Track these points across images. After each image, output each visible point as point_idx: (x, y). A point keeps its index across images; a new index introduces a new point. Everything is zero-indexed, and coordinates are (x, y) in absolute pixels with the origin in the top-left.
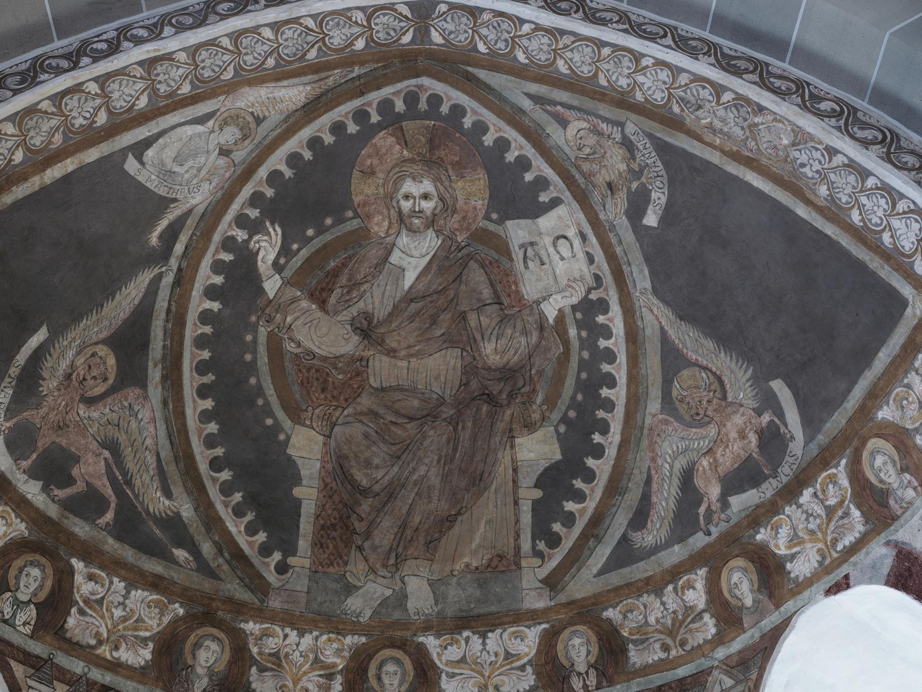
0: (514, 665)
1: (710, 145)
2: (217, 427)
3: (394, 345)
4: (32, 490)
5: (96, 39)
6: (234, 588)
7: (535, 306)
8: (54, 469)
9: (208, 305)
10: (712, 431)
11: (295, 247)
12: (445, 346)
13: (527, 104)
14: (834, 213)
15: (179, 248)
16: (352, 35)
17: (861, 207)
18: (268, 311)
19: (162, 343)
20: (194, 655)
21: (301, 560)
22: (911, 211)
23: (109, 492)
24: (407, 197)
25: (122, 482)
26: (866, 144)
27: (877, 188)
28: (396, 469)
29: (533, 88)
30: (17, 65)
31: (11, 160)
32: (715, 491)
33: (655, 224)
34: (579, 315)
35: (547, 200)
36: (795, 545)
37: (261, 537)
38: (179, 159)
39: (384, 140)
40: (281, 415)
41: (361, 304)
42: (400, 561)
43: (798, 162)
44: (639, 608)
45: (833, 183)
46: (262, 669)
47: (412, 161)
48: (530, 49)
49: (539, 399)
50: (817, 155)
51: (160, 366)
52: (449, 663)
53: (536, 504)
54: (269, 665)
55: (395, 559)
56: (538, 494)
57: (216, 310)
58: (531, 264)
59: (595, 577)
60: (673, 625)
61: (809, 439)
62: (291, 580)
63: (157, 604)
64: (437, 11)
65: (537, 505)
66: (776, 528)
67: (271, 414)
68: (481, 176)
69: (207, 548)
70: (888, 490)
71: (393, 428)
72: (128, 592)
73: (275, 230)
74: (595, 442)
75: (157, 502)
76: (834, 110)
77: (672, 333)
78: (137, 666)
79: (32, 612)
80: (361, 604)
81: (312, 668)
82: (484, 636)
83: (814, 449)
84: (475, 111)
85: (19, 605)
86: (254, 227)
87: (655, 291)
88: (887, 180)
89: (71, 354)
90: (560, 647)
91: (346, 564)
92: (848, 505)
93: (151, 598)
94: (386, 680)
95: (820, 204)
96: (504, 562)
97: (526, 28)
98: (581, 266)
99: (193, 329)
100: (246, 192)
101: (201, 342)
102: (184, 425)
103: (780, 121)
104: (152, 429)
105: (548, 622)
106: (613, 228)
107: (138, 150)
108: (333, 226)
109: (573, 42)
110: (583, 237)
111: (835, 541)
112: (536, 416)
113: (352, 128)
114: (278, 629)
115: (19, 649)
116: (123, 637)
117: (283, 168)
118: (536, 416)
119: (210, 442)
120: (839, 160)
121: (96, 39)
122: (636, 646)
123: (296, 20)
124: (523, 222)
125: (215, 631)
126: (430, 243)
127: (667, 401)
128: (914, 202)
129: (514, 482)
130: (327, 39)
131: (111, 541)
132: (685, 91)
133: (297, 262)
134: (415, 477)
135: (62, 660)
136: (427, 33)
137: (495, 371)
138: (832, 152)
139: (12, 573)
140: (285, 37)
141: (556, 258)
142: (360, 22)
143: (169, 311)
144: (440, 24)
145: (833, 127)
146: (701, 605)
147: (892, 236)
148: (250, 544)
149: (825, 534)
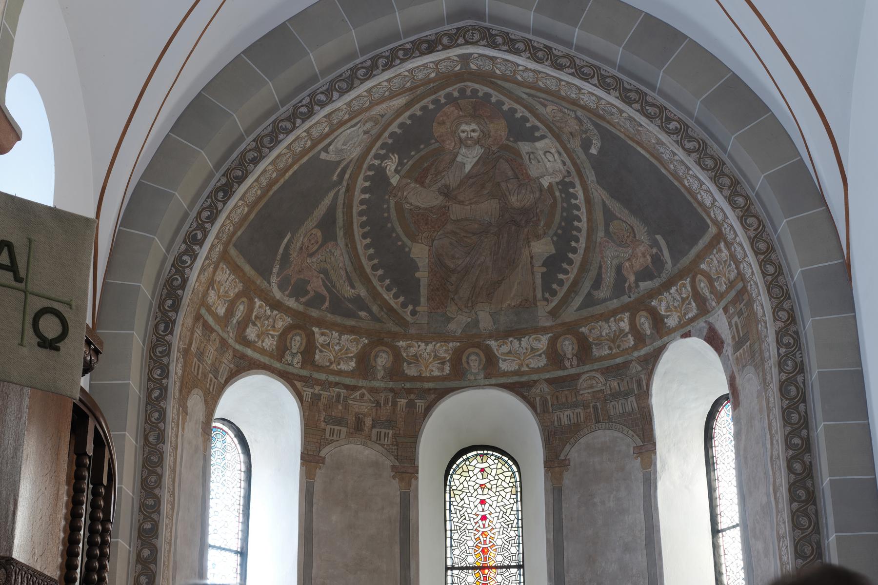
3: (462, 199)
4: (291, 303)
8: (299, 290)
9: (363, 196)
13: (525, 96)
15: (347, 176)
21: (423, 308)
23: (325, 293)
24: (463, 132)
28: (468, 259)
29: (527, 91)
32: (632, 278)
34: (560, 187)
37: (402, 299)
38: (344, 144)
39: (449, 109)
40: (405, 239)
41: (443, 181)
47: (465, 116)
49: (542, 223)
52: (503, 354)
53: (543, 274)
56: (544, 270)
61: (674, 265)
63: (355, 340)
66: (660, 301)
67: (401, 240)
69: (375, 309)
76: (676, 128)
79: (299, 356)
80: (455, 327)
81: (434, 360)
82: (520, 340)
85: (293, 355)
86: (383, 158)
87: (598, 182)
90: (558, 345)
94: (472, 364)
97: (520, 68)
99: (356, 208)
101: (361, 214)
102: (357, 253)
104: (342, 259)
106: (574, 151)
107: (326, 149)
110: (560, 154)
111: (685, 314)
112: (541, 232)
113: (431, 107)
115: (297, 375)
116: (341, 358)
118: (541, 232)
119: (370, 258)
120: (676, 158)
124: (527, 143)
125: (384, 348)
131: (329, 315)
133: (407, 167)
134: (479, 262)
135: (316, 375)
136: (468, 64)
138: (675, 154)
139: (288, 341)
143: (344, 203)
146: (627, 330)
148: (396, 303)
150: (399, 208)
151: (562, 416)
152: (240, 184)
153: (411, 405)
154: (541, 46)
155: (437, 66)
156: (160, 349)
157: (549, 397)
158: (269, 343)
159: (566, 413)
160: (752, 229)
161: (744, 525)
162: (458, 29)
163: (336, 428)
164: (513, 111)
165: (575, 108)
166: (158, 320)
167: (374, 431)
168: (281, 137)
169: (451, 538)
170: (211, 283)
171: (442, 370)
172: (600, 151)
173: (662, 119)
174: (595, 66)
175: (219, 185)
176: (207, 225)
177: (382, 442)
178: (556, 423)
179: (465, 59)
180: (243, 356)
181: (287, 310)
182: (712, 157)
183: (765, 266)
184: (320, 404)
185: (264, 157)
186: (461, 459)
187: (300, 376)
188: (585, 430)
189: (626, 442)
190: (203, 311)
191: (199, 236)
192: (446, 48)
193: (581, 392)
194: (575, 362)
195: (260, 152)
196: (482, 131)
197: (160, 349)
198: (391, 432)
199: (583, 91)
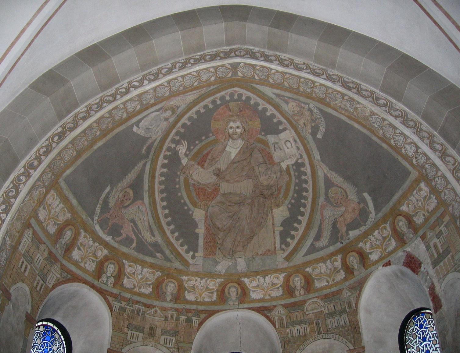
0: (275, 287)
1: (341, 113)
2: (168, 211)
4: (109, 239)
5: (121, 87)
6: (177, 265)
7: (278, 164)
10: (343, 209)
11: (192, 147)
12: (247, 178)
14: (384, 139)
16: (210, 76)
17: (394, 139)
18: (183, 170)
19: (148, 185)
20: (166, 289)
21: (200, 254)
22: (412, 143)
23: (133, 237)
24: (231, 128)
25: (137, 231)
26: (396, 117)
27: (400, 134)
30: (95, 100)
31: (96, 135)
32: (344, 229)
33: (321, 138)
34: (294, 168)
35: (282, 128)
36: (372, 249)
41: (216, 165)
42: (234, 253)
43: (372, 121)
44: (318, 268)
45: (384, 130)
46: (189, 292)
48: (274, 78)
50: (378, 120)
51: (147, 193)
52: (252, 287)
54: (191, 290)
55: (232, 253)
56: (281, 228)
57: (166, 172)
58: (277, 150)
59: (302, 257)
60: (330, 273)
62: (197, 261)
64: (240, 66)
65: (281, 233)
66: (365, 243)
67: (187, 205)
68: (258, 120)
69: (167, 252)
70: (404, 233)
71: (229, 207)
72: (143, 269)
73: (185, 143)
74: (301, 210)
75: (148, 237)
76: (384, 103)
77: (328, 175)
78: (147, 293)
79: (112, 279)
82: (264, 277)
83: (380, 215)
84: (254, 99)
85: (108, 278)
86: (178, 143)
87: (322, 161)
88: (403, 131)
89: (118, 193)
91: (215, 254)
92: (390, 238)
93: (150, 270)
94: (231, 294)
95: (380, 136)
96: (271, 252)
98: (294, 151)
100: (174, 131)
101: (160, 183)
103: (365, 108)
105: (287, 272)
107: (137, 123)
108: (205, 139)
109: (290, 77)
110: (295, 141)
113: (211, 106)
114: (193, 278)
116: (142, 285)
117: (187, 122)
120: (386, 122)
121: (121, 87)
122: (317, 280)
123: (190, 74)
126: (240, 143)
127: (327, 198)
128: (413, 140)
129: (273, 224)
130: (201, 78)
131: (136, 253)
132: (331, 95)
137: (265, 186)
138: (384, 120)
140: (186, 79)
141: (285, 148)
142: (212, 71)
143: (149, 173)
144: (241, 70)
145: (384, 111)
146: (340, 267)
147: (405, 150)
149: (382, 246)
150: (186, 180)
152: (70, 132)
153: (189, 321)
154: (287, 59)
157: (284, 318)
158: (91, 266)
159: (296, 328)
160: (451, 164)
162: (231, 49)
163: (136, 333)
164: (265, 110)
165: (309, 101)
167: (163, 338)
168: (105, 105)
170: (41, 202)
171: (211, 297)
172: (324, 136)
173: (373, 98)
174: (324, 69)
175: (56, 132)
176: (42, 157)
177: (168, 345)
178: (290, 336)
179: (235, 66)
180: (69, 272)
182: (412, 120)
184: (125, 314)
185: (91, 116)
187: (112, 293)
188: (311, 339)
190: (33, 221)
192: (222, 58)
193: (307, 313)
194: (302, 292)
195: (89, 113)
196: (243, 128)
199: (316, 84)
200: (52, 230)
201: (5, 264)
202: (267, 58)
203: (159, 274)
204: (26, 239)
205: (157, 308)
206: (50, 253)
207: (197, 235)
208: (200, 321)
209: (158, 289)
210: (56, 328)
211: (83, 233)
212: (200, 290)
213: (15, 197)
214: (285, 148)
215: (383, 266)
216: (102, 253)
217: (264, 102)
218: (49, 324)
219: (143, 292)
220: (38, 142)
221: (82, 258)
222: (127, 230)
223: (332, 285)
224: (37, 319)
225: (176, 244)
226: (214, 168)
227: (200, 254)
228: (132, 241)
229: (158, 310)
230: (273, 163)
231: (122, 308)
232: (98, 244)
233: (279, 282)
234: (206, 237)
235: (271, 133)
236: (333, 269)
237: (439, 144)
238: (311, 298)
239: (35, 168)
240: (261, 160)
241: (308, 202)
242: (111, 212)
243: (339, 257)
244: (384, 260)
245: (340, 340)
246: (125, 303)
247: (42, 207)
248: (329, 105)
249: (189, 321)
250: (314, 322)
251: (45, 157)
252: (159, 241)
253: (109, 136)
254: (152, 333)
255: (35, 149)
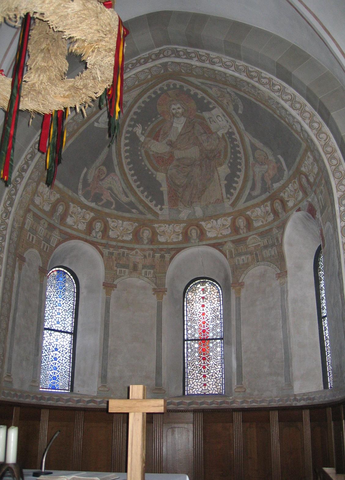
4: (93, 205)
6: (150, 216)
10: (266, 166)
11: (146, 128)
20: (143, 235)
23: (112, 200)
24: (174, 109)
34: (228, 135)
36: (289, 198)
40: (153, 170)
41: (168, 138)
52: (208, 228)
55: (191, 203)
56: (226, 182)
69: (141, 208)
71: (184, 169)
72: (123, 223)
75: (124, 199)
76: (278, 89)
77: (253, 141)
79: (100, 233)
82: (216, 220)
83: (291, 172)
84: (186, 87)
85: (97, 232)
86: (134, 126)
91: (178, 205)
94: (193, 235)
98: (225, 123)
101: (126, 158)
107: (97, 120)
110: (224, 116)
113: (153, 96)
117: (137, 110)
123: (130, 77)
125: (146, 228)
126: (183, 120)
129: (219, 179)
133: (147, 132)
141: (218, 121)
146: (270, 211)
150: (146, 152)
151: (240, 260)
153: (162, 257)
154: (204, 54)
155: (150, 70)
156: (3, 227)
157: (233, 250)
158: (82, 227)
160: (323, 140)
161: (73, 278)
162: (160, 50)
163: (123, 269)
164: (196, 94)
165: (226, 87)
166: (2, 212)
167: (144, 271)
169: (187, 324)
170: (35, 192)
171: (178, 238)
173: (270, 85)
174: (317, 137)
177: (148, 276)
178: (237, 264)
179: (165, 65)
180: (66, 233)
181: (92, 209)
182: (299, 103)
183: (331, 161)
184: (113, 257)
186: (192, 284)
188: (252, 266)
189: (272, 270)
190: (31, 207)
191: (25, 168)
192: (153, 60)
193: (249, 246)
194: (245, 231)
196: (183, 108)
197: (3, 227)
198: (152, 271)
200: (47, 208)
201: (17, 240)
202: (188, 55)
203: (136, 224)
204: (29, 220)
205: (137, 250)
206: (49, 224)
207: (162, 193)
208: (171, 256)
209: (137, 236)
210: (66, 271)
211: (72, 205)
212: (169, 233)
213: (15, 194)
214: (218, 121)
215: (297, 211)
216: (90, 216)
217: (194, 89)
218: (61, 269)
219: (125, 239)
220: (25, 150)
221: (74, 222)
222: (106, 196)
223: (266, 224)
224: (48, 269)
225: (147, 201)
226: (166, 140)
227: (166, 207)
228: (111, 204)
229: (138, 251)
230: (211, 133)
231: (110, 253)
232: (85, 210)
233: (228, 223)
234: (169, 193)
235: (205, 111)
236: (266, 212)
237: (318, 122)
238: (251, 235)
239: (25, 171)
240: (202, 131)
241: (242, 161)
242: (91, 186)
243: (269, 203)
244: (297, 207)
245: (272, 266)
246: (113, 249)
247: (36, 195)
248: (240, 90)
249: (162, 257)
250: (254, 253)
251: (31, 161)
252: (133, 201)
253: (77, 135)
254: (135, 268)
255: (24, 156)
